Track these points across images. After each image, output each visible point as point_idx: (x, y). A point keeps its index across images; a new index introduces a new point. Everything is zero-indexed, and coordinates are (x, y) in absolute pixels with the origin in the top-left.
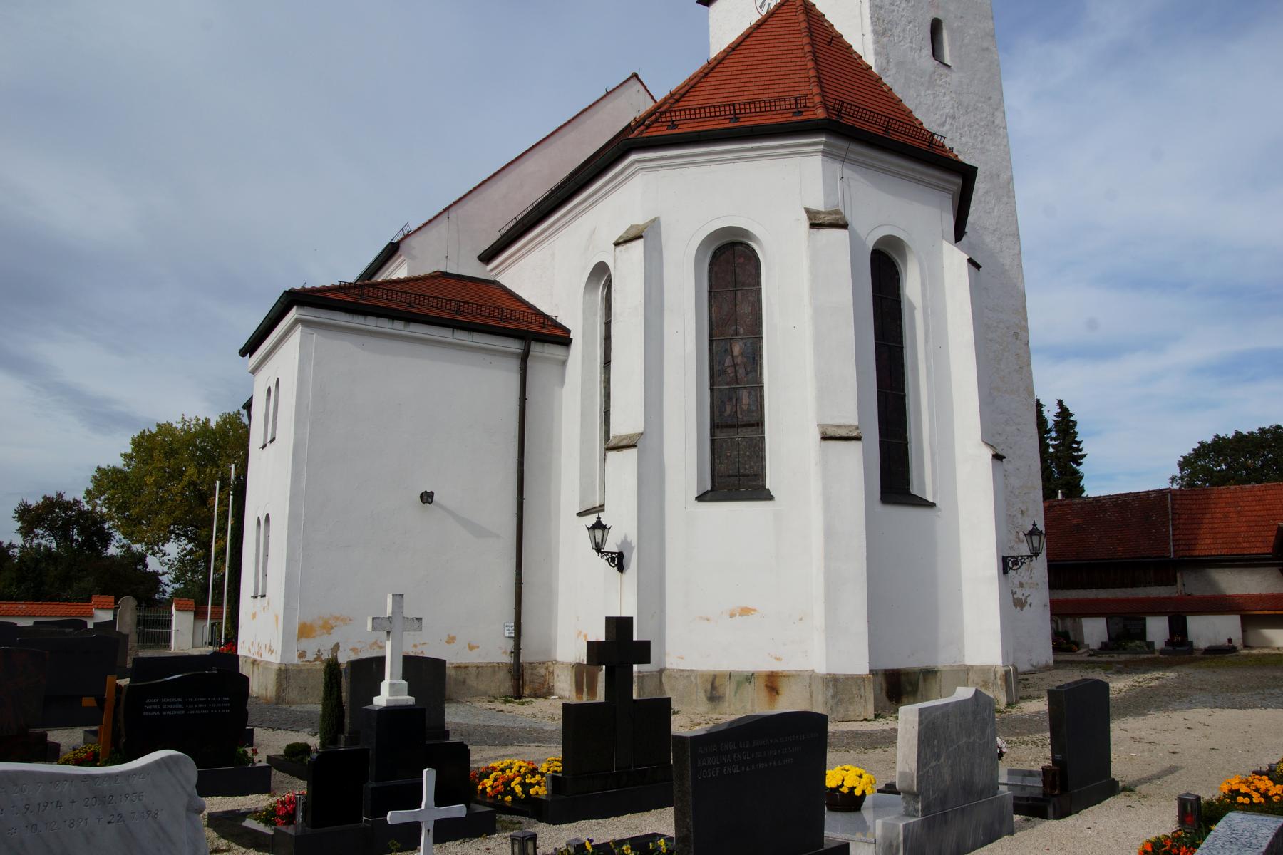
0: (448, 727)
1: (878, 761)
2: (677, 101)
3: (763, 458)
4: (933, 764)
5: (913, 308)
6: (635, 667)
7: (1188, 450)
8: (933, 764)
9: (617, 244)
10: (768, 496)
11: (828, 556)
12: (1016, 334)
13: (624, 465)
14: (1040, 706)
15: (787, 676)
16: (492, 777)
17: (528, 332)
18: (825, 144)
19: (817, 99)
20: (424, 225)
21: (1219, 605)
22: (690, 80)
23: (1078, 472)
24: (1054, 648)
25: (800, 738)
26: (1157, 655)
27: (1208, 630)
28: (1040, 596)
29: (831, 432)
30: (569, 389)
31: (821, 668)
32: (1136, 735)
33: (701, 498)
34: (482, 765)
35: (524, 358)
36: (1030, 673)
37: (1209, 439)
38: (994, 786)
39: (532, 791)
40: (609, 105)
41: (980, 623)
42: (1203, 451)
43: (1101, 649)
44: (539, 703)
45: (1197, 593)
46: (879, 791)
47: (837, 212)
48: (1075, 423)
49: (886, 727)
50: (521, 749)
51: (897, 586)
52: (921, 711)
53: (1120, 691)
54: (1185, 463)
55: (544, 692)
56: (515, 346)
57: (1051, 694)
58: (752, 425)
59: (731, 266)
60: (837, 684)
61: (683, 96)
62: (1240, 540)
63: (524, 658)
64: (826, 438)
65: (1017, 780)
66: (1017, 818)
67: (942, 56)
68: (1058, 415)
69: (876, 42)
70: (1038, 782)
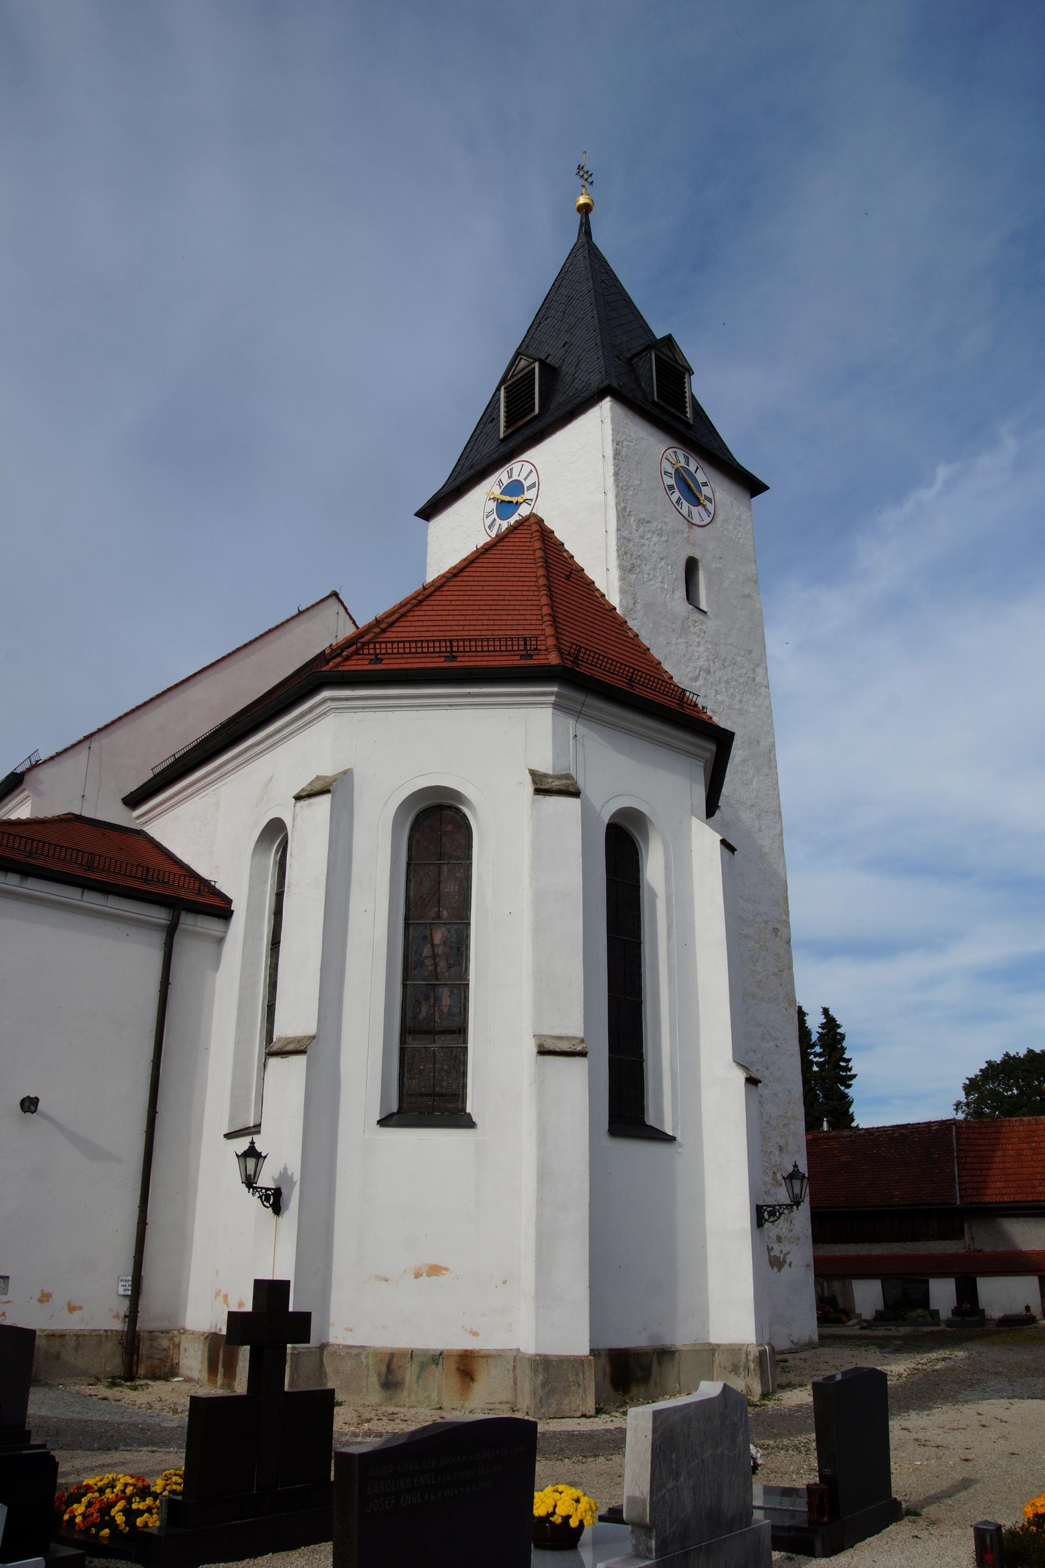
0: (31, 1423)
1: (600, 1475)
2: (384, 631)
3: (464, 1074)
4: (670, 1485)
5: (654, 896)
6: (289, 1345)
7: (974, 1071)
8: (670, 1485)
9: (298, 798)
10: (467, 1122)
11: (541, 1201)
12: (776, 931)
13: (288, 1078)
14: (801, 1397)
15: (486, 1356)
16: (85, 1500)
17: (178, 899)
18: (557, 695)
19: (551, 642)
20: (58, 754)
21: (1015, 1264)
22: (402, 605)
23: (846, 1096)
24: (819, 1319)
25: (503, 1451)
26: (942, 1327)
27: (1004, 1295)
28: (801, 1255)
29: (550, 1045)
30: (225, 978)
31: (529, 1347)
32: (921, 1435)
33: (383, 1122)
34: (72, 1479)
35: (171, 932)
36: (790, 1351)
37: (998, 1058)
38: (747, 1510)
39: (139, 1521)
40: (299, 628)
41: (727, 1293)
42: (991, 1071)
43: (875, 1319)
44: (159, 1388)
45: (987, 1249)
46: (601, 1519)
47: (568, 777)
48: (843, 1037)
49: (610, 1426)
50: (128, 1456)
51: (627, 1243)
52: (656, 1414)
53: (900, 1376)
54: (972, 1086)
55: (166, 1371)
56: (160, 916)
57: (816, 1386)
58: (453, 1032)
59: (437, 832)
60: (549, 1370)
61: (391, 625)
62: (1036, 1183)
64: (543, 1052)
65: (776, 1502)
66: (776, 1555)
67: (698, 601)
68: (823, 1026)
69: (622, 579)
70: (802, 1505)
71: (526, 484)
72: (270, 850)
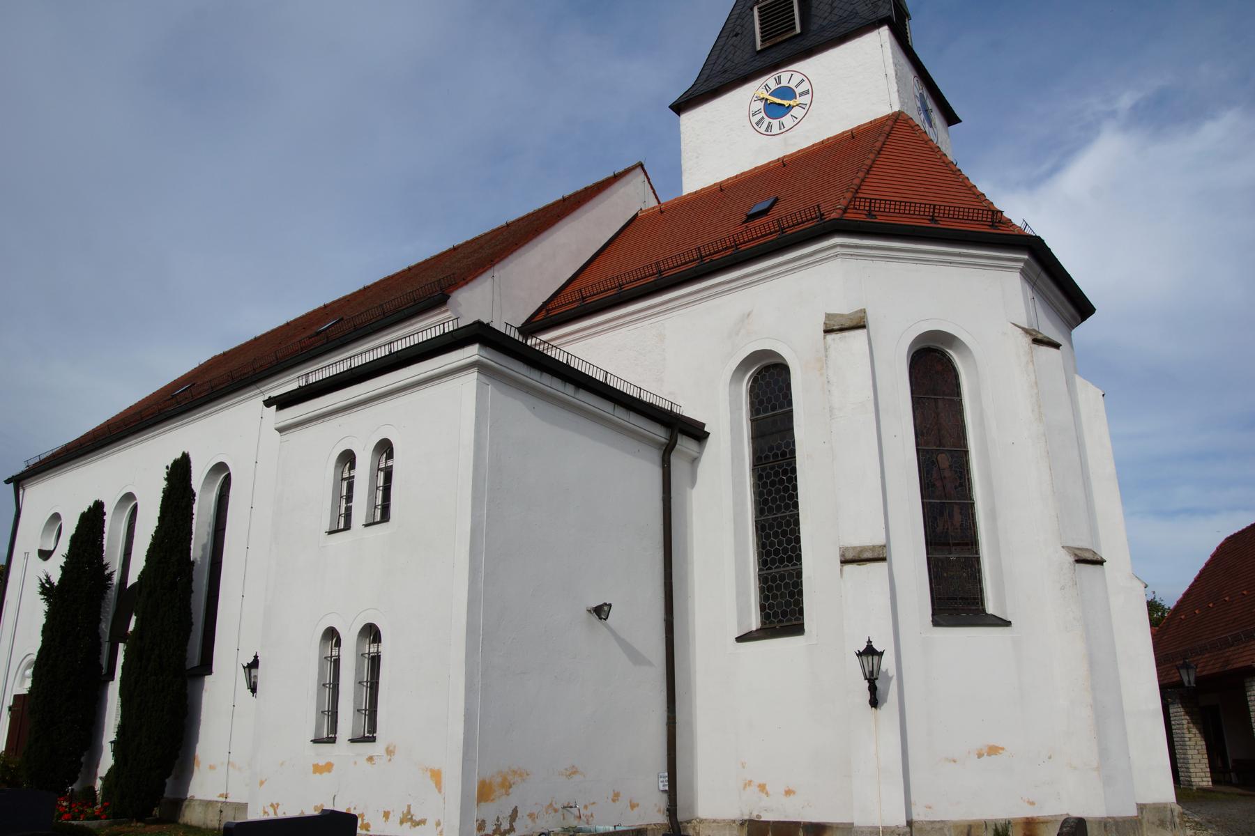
35: (667, 452)
56: (659, 433)
63: (681, 817)
71: (798, 91)
72: (742, 379)
